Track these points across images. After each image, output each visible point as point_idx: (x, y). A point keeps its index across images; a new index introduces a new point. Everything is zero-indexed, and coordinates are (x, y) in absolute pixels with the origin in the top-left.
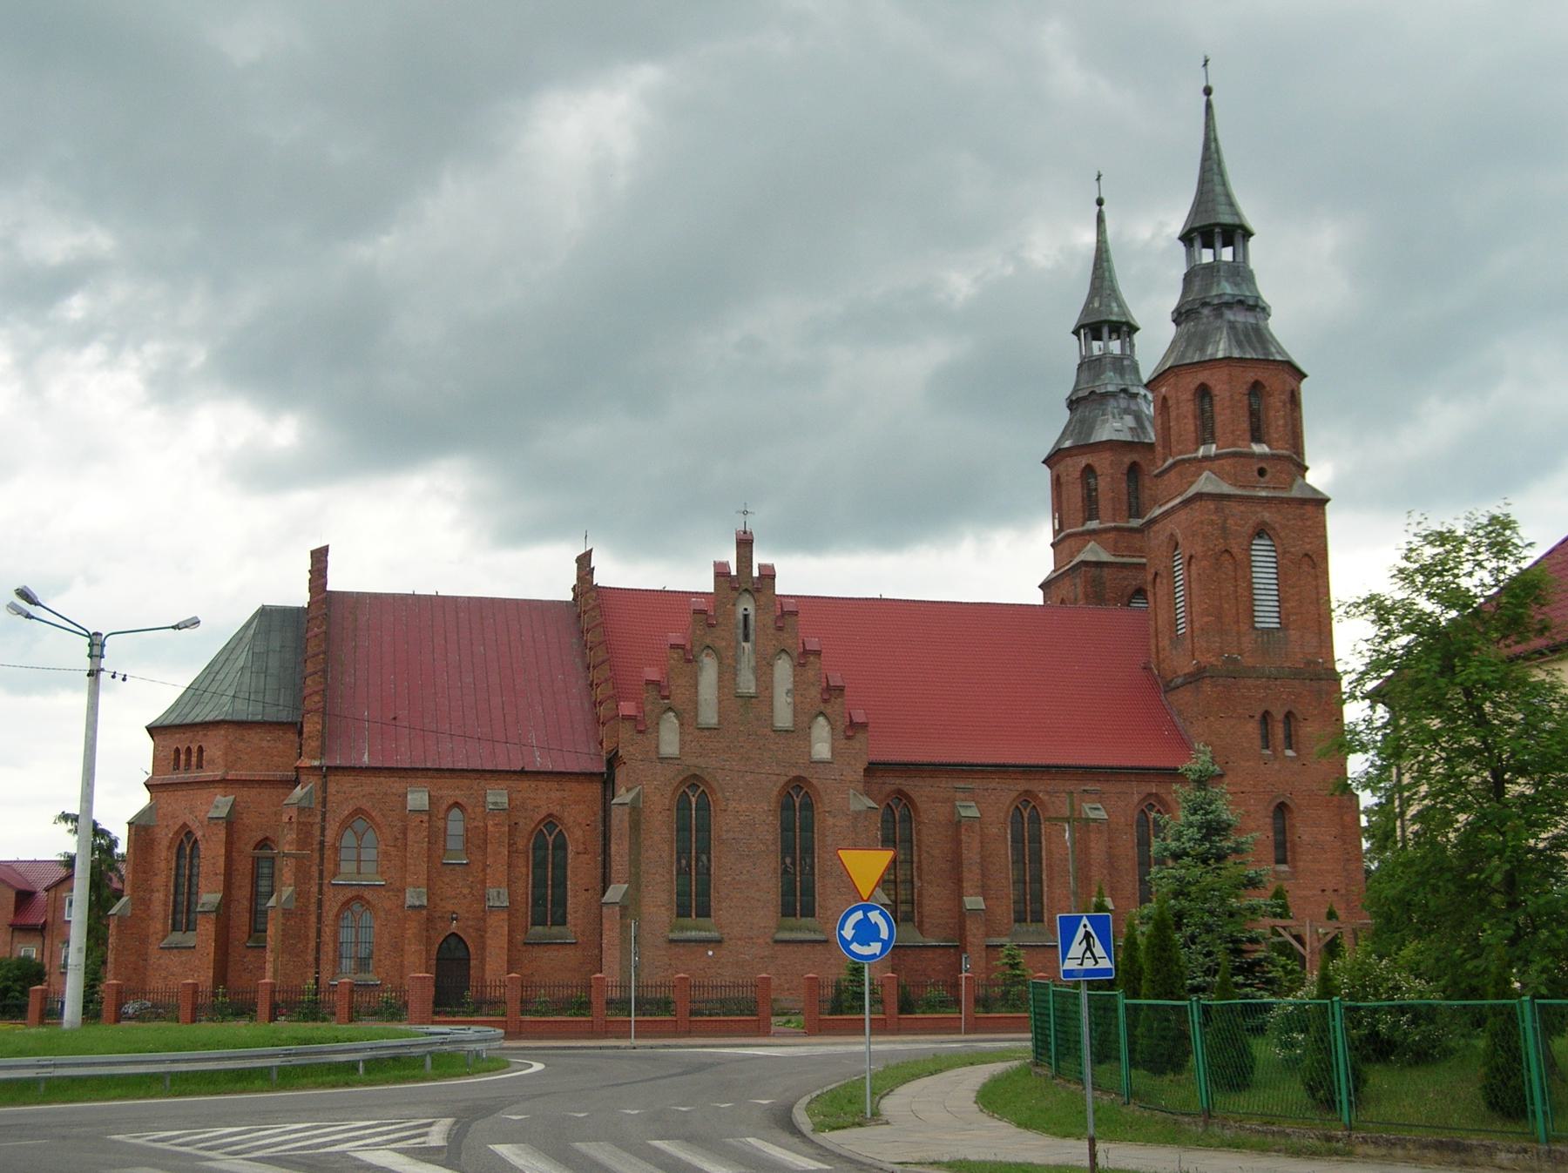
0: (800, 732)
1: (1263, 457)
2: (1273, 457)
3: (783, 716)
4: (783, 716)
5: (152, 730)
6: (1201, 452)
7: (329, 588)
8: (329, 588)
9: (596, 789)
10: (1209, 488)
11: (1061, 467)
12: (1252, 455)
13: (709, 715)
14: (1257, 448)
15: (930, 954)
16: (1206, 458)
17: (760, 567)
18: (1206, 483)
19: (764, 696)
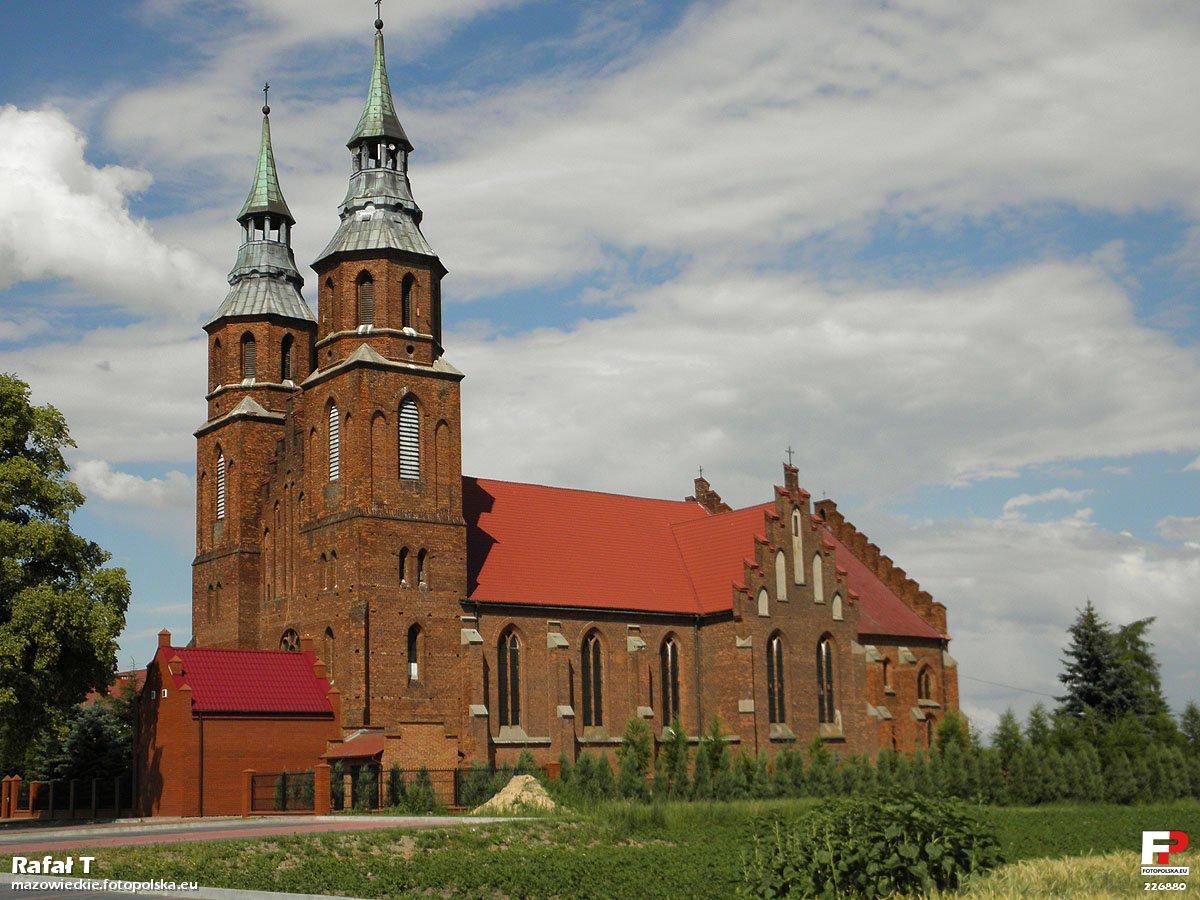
0: (826, 604)
1: (411, 338)
2: (418, 339)
3: (819, 596)
4: (819, 596)
5: (195, 435)
6: (361, 329)
7: (1144, 833)
8: (1144, 833)
9: (882, 665)
10: (368, 359)
11: (219, 334)
12: (403, 336)
13: (782, 593)
14: (408, 331)
15: (259, 426)
16: (364, 335)
17: (816, 504)
18: (364, 353)
19: (808, 585)
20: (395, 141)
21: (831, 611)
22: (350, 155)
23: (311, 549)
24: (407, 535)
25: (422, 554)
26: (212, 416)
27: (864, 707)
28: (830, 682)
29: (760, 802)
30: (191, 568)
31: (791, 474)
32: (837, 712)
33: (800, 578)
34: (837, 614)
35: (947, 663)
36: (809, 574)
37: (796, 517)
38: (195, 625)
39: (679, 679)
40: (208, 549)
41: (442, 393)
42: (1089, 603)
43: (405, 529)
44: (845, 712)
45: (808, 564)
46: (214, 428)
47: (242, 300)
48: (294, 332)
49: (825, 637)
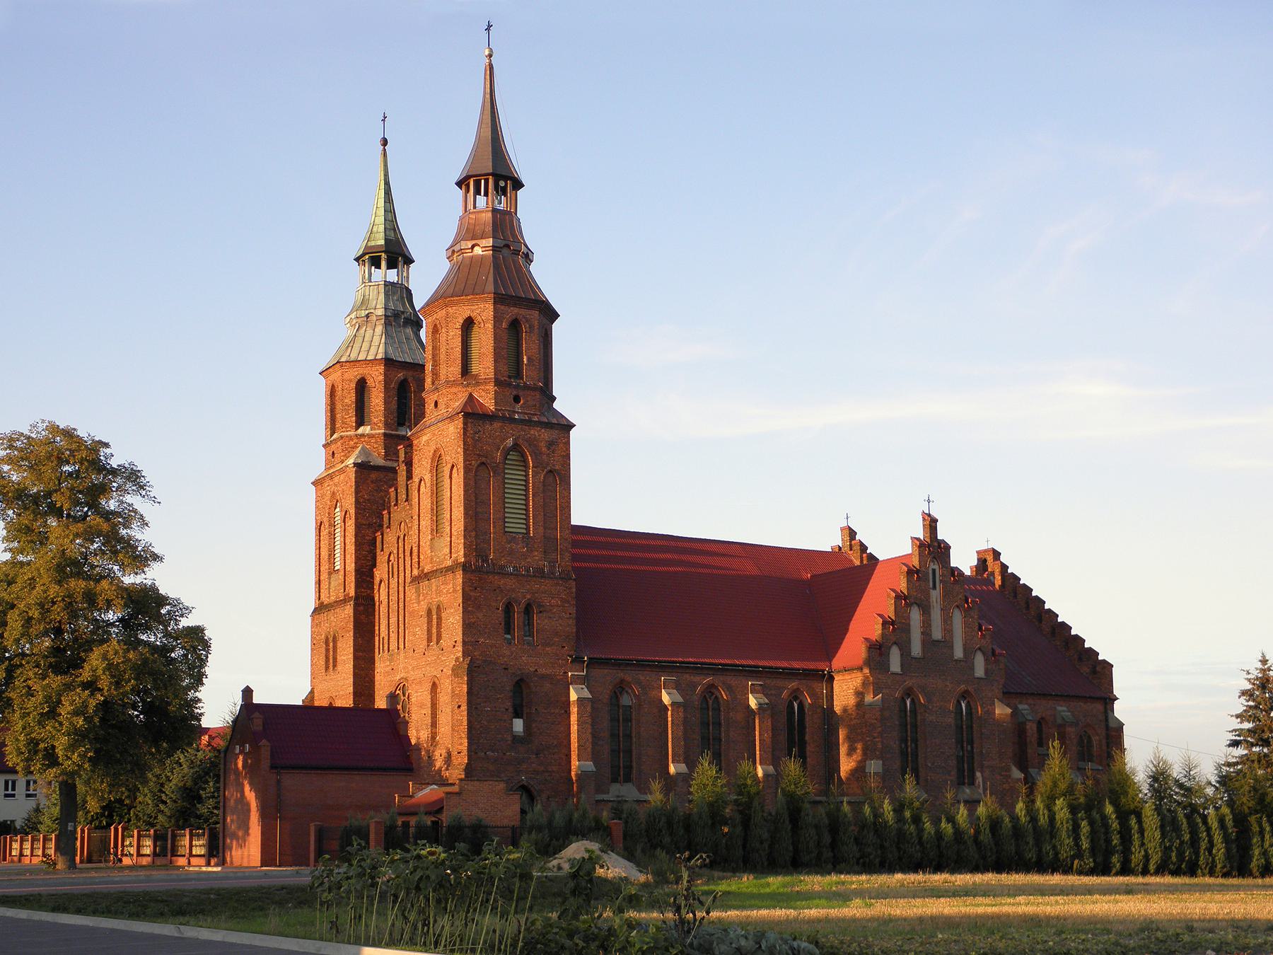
3: (959, 653)
4: (959, 653)
13: (916, 649)
19: (947, 643)
20: (506, 178)
21: (972, 669)
22: (460, 193)
23: (419, 603)
24: (513, 590)
25: (528, 610)
26: (329, 465)
27: (1009, 770)
28: (971, 742)
29: (621, 834)
30: (310, 619)
31: (931, 524)
32: (978, 774)
33: (937, 634)
34: (980, 671)
35: (1112, 724)
36: (948, 630)
37: (934, 571)
38: (313, 678)
39: (807, 738)
40: (326, 600)
41: (551, 444)
42: (1264, 661)
43: (510, 583)
44: (987, 773)
45: (947, 620)
46: (331, 477)
47: (357, 346)
48: (523, 312)
49: (965, 695)
